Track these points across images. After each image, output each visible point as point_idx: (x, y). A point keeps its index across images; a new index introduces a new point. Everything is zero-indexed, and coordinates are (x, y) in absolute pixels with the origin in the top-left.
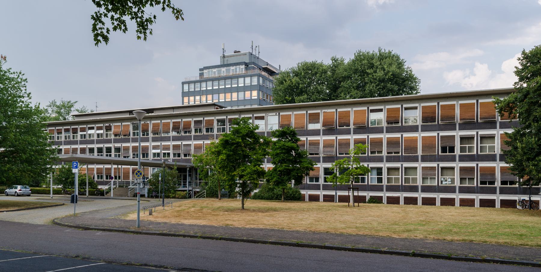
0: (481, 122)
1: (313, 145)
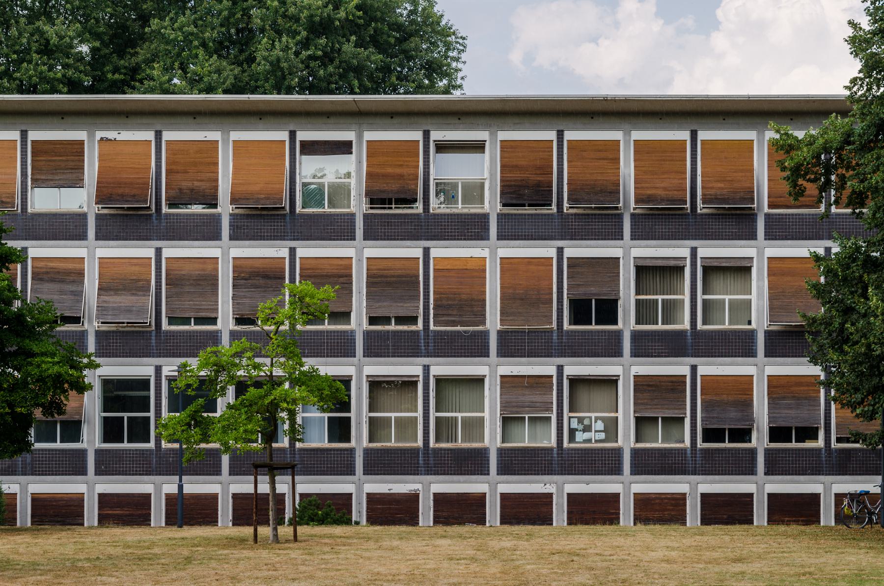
0: (705, 211)
1: (52, 280)
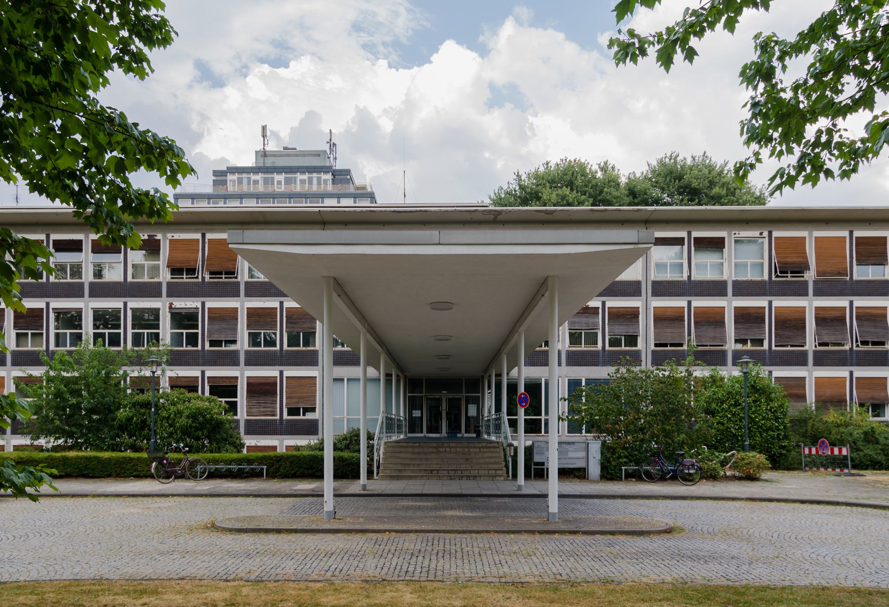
1: (868, 320)
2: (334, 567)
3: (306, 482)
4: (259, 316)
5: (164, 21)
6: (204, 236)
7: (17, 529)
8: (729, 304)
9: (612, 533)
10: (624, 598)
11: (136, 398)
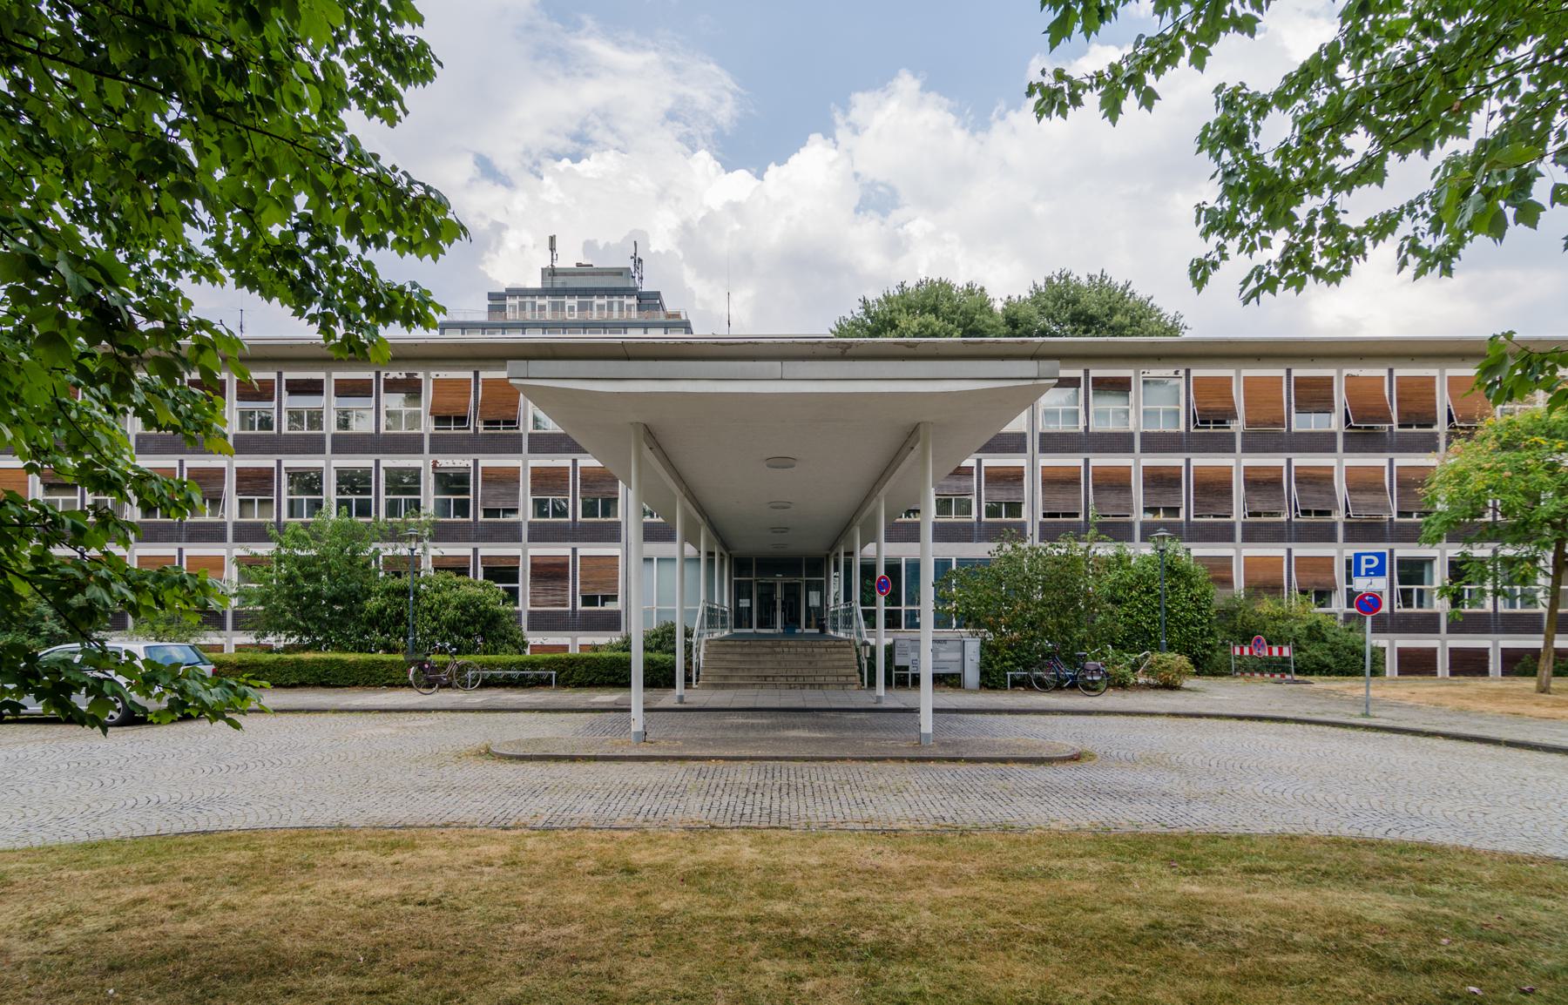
1: (1310, 483)
2: (646, 808)
3: (606, 692)
4: (546, 477)
5: (423, 48)
6: (476, 374)
7: (233, 756)
8: (1136, 463)
9: (1004, 761)
10: (1033, 852)
11: (391, 582)
